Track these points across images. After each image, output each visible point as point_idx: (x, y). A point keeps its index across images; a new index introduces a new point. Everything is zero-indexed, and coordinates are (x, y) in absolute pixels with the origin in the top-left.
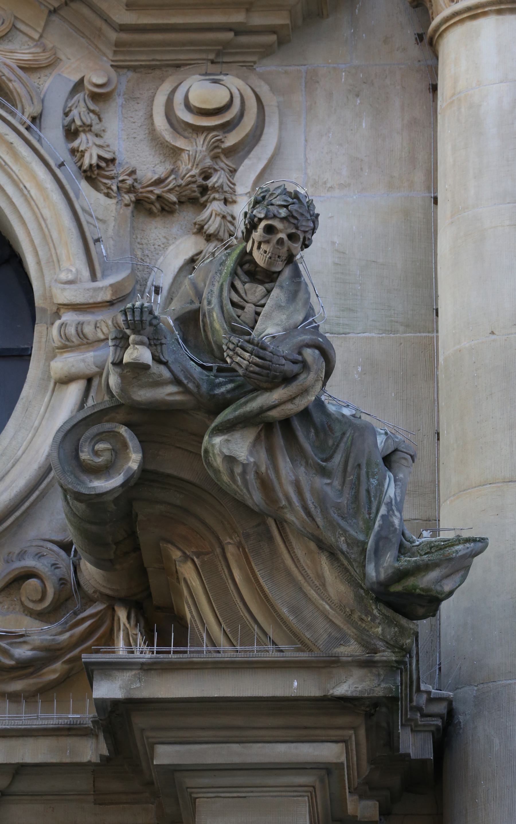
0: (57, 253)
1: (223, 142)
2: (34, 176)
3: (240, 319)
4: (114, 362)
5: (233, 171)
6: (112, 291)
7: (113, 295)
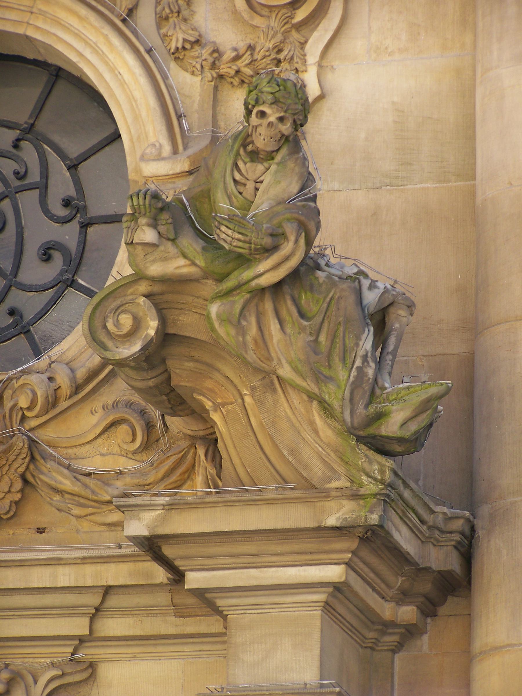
0: (145, 130)
1: (292, 18)
2: (126, 63)
3: (242, 196)
4: (127, 242)
5: (303, 44)
6: (190, 162)
7: (191, 165)
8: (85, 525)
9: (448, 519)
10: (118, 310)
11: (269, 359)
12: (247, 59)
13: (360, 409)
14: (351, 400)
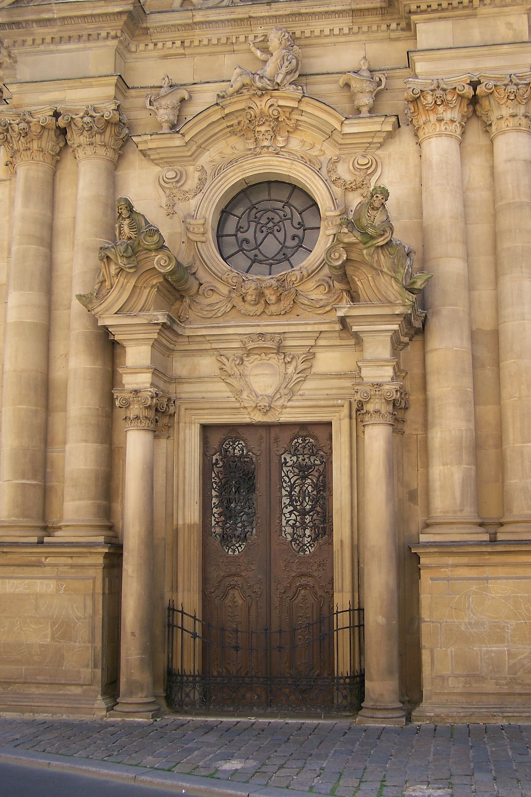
5: (370, 180)
8: (311, 314)
9: (421, 313)
10: (335, 252)
11: (380, 266)
12: (354, 184)
13: (408, 280)
14: (405, 278)
